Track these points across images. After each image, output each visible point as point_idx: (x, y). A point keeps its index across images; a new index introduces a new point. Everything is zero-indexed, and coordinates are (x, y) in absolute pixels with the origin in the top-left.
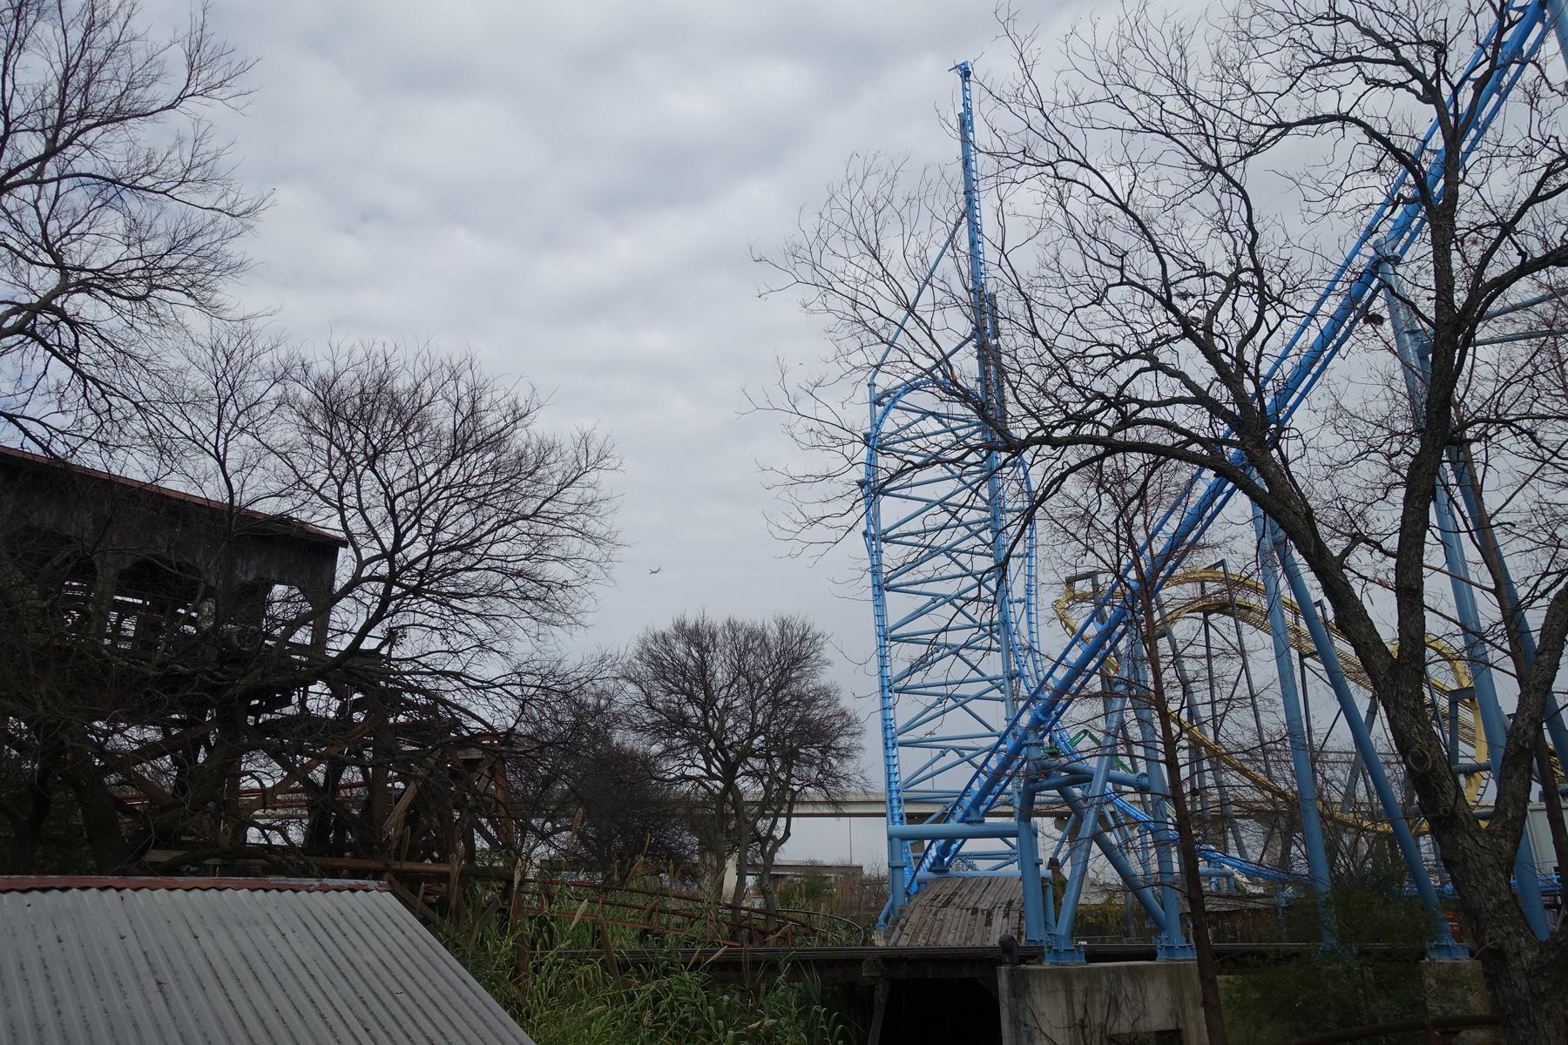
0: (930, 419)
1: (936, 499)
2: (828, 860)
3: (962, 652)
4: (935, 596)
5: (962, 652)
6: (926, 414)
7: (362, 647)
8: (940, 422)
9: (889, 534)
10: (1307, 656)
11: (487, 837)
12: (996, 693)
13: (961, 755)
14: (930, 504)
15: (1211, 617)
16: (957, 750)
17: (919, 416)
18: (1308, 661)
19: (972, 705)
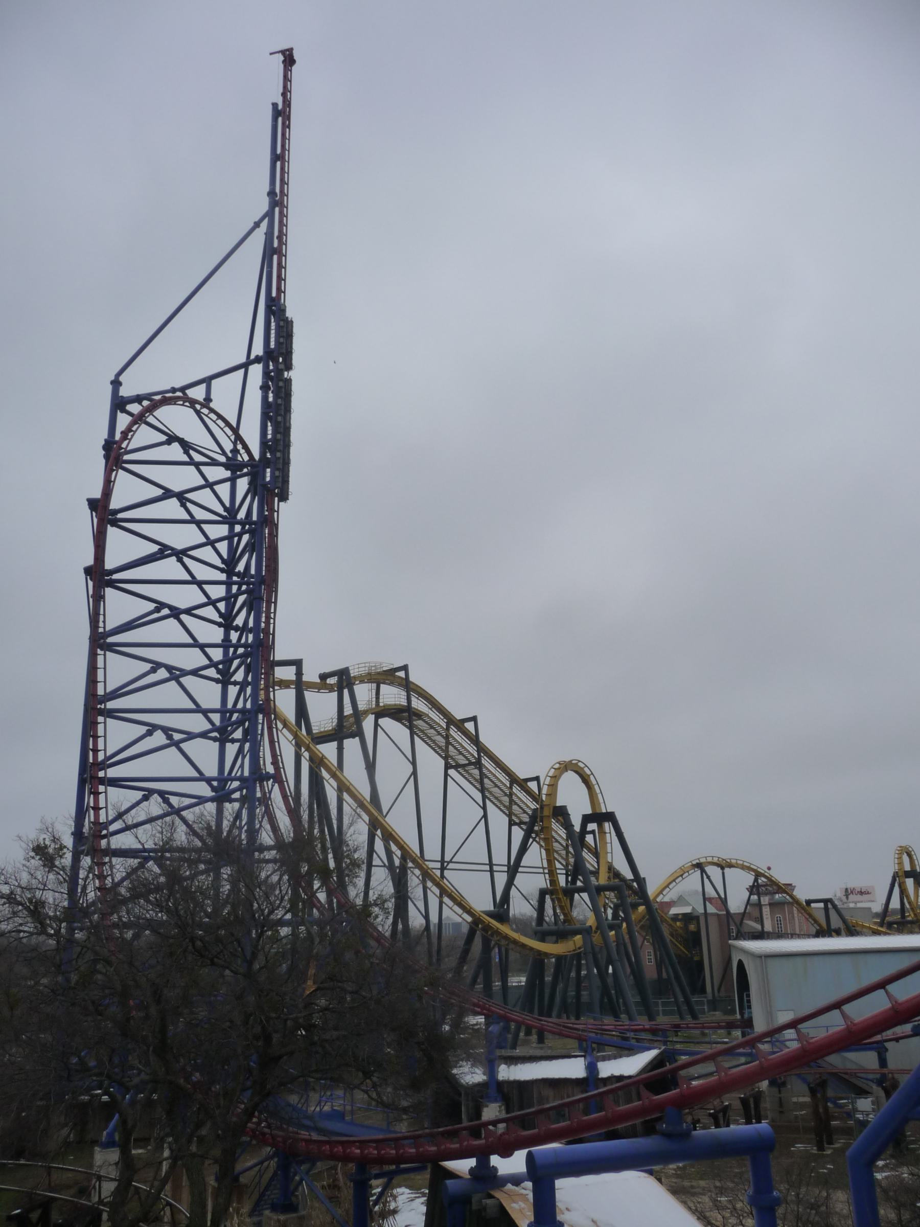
0: (176, 445)
1: (177, 489)
2: (613, 1060)
3: (183, 617)
4: (161, 605)
5: (183, 617)
6: (172, 439)
7: (182, 813)
8: (186, 452)
9: (120, 516)
10: (452, 767)
11: (333, 879)
12: (212, 672)
13: (169, 737)
14: (168, 494)
15: (382, 721)
16: (166, 730)
17: (164, 438)
18: (452, 772)
19: (187, 681)
